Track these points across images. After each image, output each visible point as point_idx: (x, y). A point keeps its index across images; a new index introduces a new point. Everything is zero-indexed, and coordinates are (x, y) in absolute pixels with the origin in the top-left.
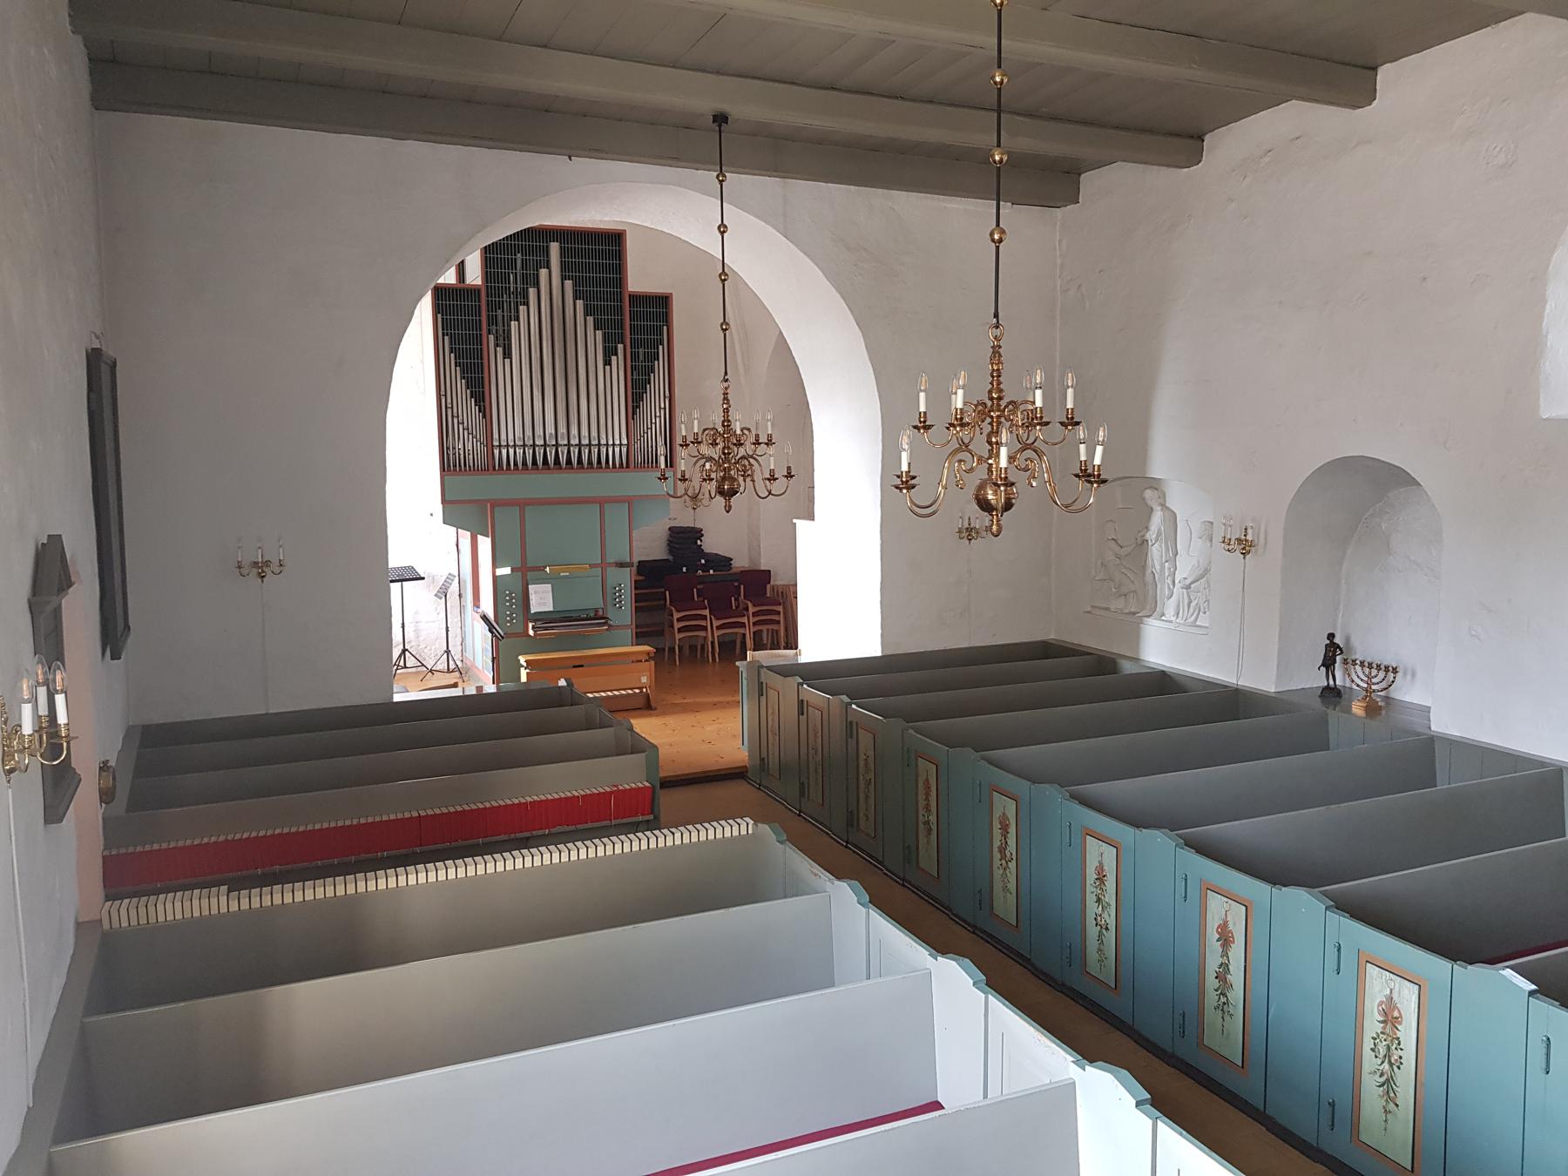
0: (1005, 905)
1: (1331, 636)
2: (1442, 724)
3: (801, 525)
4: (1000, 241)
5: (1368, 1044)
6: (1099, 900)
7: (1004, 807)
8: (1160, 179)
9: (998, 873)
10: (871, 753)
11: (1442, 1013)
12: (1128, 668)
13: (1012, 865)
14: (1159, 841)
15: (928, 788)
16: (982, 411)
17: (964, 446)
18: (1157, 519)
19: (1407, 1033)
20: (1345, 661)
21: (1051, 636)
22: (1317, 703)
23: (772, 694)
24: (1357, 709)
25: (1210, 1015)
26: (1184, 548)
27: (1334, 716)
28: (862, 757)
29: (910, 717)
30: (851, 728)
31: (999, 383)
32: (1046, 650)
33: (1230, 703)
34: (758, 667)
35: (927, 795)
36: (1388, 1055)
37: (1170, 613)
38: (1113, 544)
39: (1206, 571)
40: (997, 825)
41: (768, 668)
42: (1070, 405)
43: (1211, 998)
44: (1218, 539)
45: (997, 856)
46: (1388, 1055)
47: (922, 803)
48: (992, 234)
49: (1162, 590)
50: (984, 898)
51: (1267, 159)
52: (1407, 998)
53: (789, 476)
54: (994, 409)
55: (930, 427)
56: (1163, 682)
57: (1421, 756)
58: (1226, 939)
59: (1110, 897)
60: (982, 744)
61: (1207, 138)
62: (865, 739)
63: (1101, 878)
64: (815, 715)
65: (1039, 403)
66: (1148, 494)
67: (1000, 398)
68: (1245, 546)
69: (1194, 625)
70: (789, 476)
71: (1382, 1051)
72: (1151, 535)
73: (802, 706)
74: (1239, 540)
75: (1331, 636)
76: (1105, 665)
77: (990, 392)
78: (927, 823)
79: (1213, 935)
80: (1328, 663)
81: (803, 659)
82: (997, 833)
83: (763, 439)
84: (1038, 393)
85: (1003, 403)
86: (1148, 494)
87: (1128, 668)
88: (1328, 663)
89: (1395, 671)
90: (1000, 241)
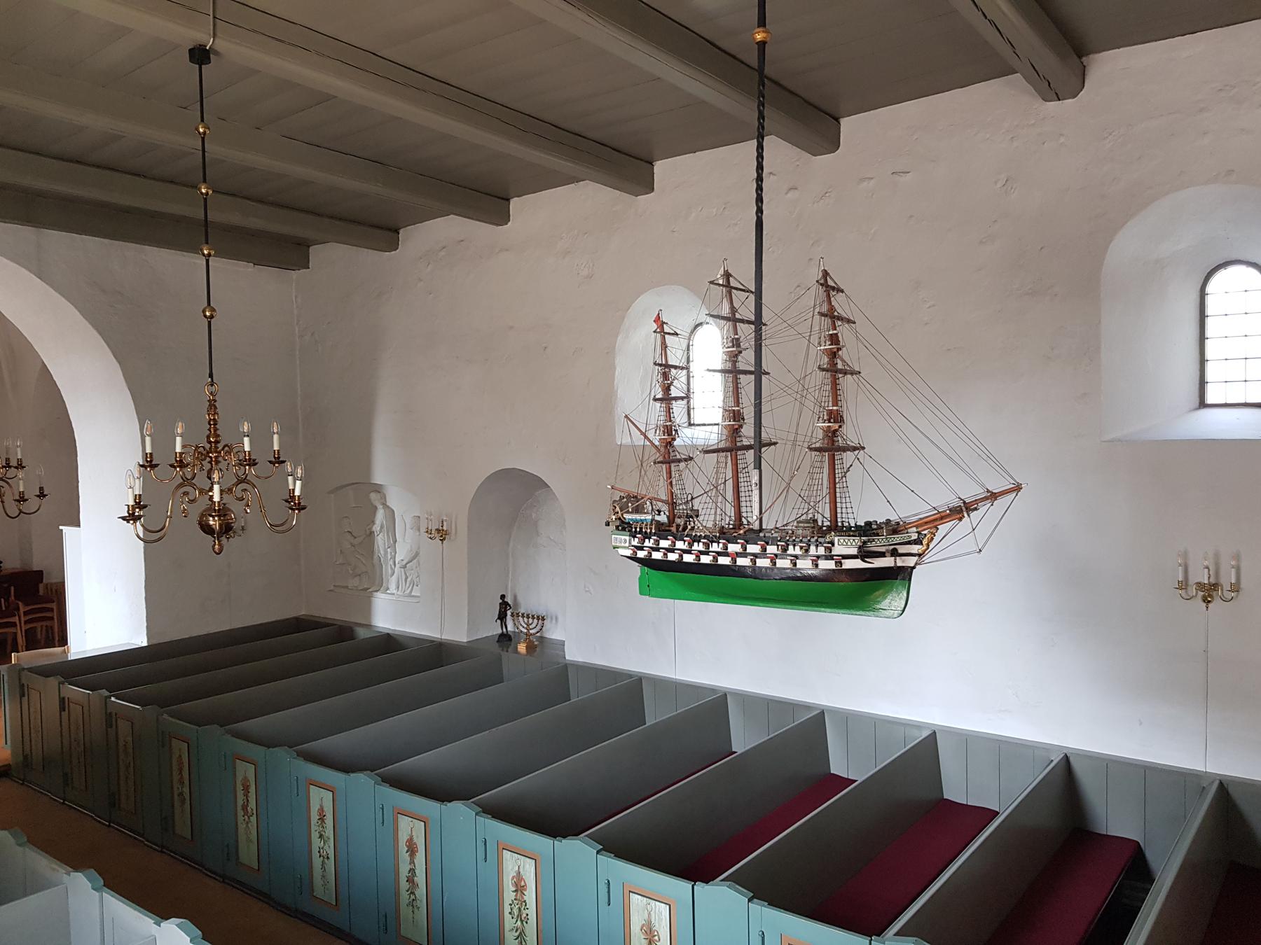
0: (248, 854)
1: (503, 597)
2: (574, 654)
3: (66, 530)
4: (212, 317)
5: (507, 909)
6: (321, 836)
7: (245, 771)
8: (368, 258)
9: (242, 827)
10: (130, 739)
11: (549, 875)
12: (362, 633)
13: (254, 819)
14: (363, 781)
15: (181, 763)
16: (201, 455)
17: (186, 481)
18: (380, 515)
19: (530, 896)
20: (512, 615)
21: (303, 612)
22: (496, 648)
23: (34, 695)
24: (522, 648)
25: (405, 911)
26: (400, 540)
27: (507, 657)
28: (121, 743)
29: (163, 702)
30: (110, 718)
31: (216, 430)
32: (298, 625)
33: (436, 654)
34: (19, 671)
35: (181, 770)
36: (520, 915)
37: (393, 589)
38: (349, 536)
39: (417, 554)
40: (240, 787)
41: (30, 670)
42: (276, 448)
43: (404, 896)
44: (423, 530)
45: (240, 813)
46: (520, 915)
47: (176, 777)
48: (204, 312)
49: (387, 570)
50: (232, 851)
51: (442, 253)
52: (528, 868)
53: (42, 495)
54: (212, 450)
55: (156, 465)
56: (389, 642)
57: (560, 678)
58: (412, 850)
59: (329, 832)
60: (225, 720)
61: (401, 231)
62: (123, 727)
63: (322, 819)
64: (76, 710)
65: (247, 448)
66: (373, 496)
67: (217, 442)
68: (442, 534)
69: (410, 596)
70: (42, 495)
71: (516, 912)
72: (376, 528)
73: (63, 703)
74: (438, 530)
75: (503, 597)
76: (344, 633)
77: (208, 437)
78: (181, 794)
79: (403, 848)
80: (502, 617)
81: (72, 657)
82: (240, 794)
83: (14, 463)
84: (246, 440)
85: (220, 446)
86: (373, 496)
87: (362, 633)
88: (502, 617)
89: (543, 619)
90: (212, 317)
